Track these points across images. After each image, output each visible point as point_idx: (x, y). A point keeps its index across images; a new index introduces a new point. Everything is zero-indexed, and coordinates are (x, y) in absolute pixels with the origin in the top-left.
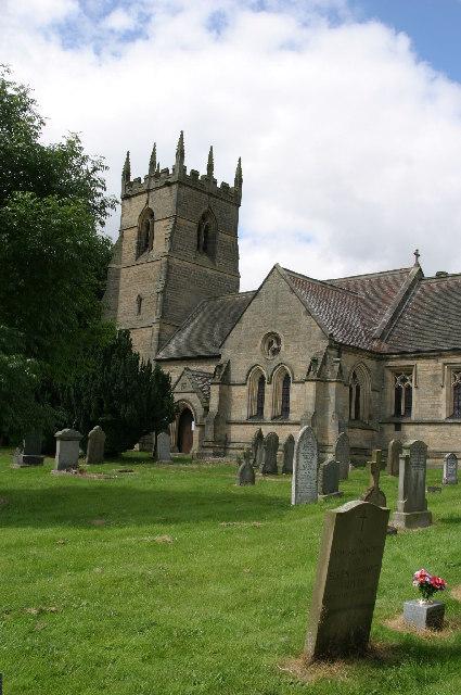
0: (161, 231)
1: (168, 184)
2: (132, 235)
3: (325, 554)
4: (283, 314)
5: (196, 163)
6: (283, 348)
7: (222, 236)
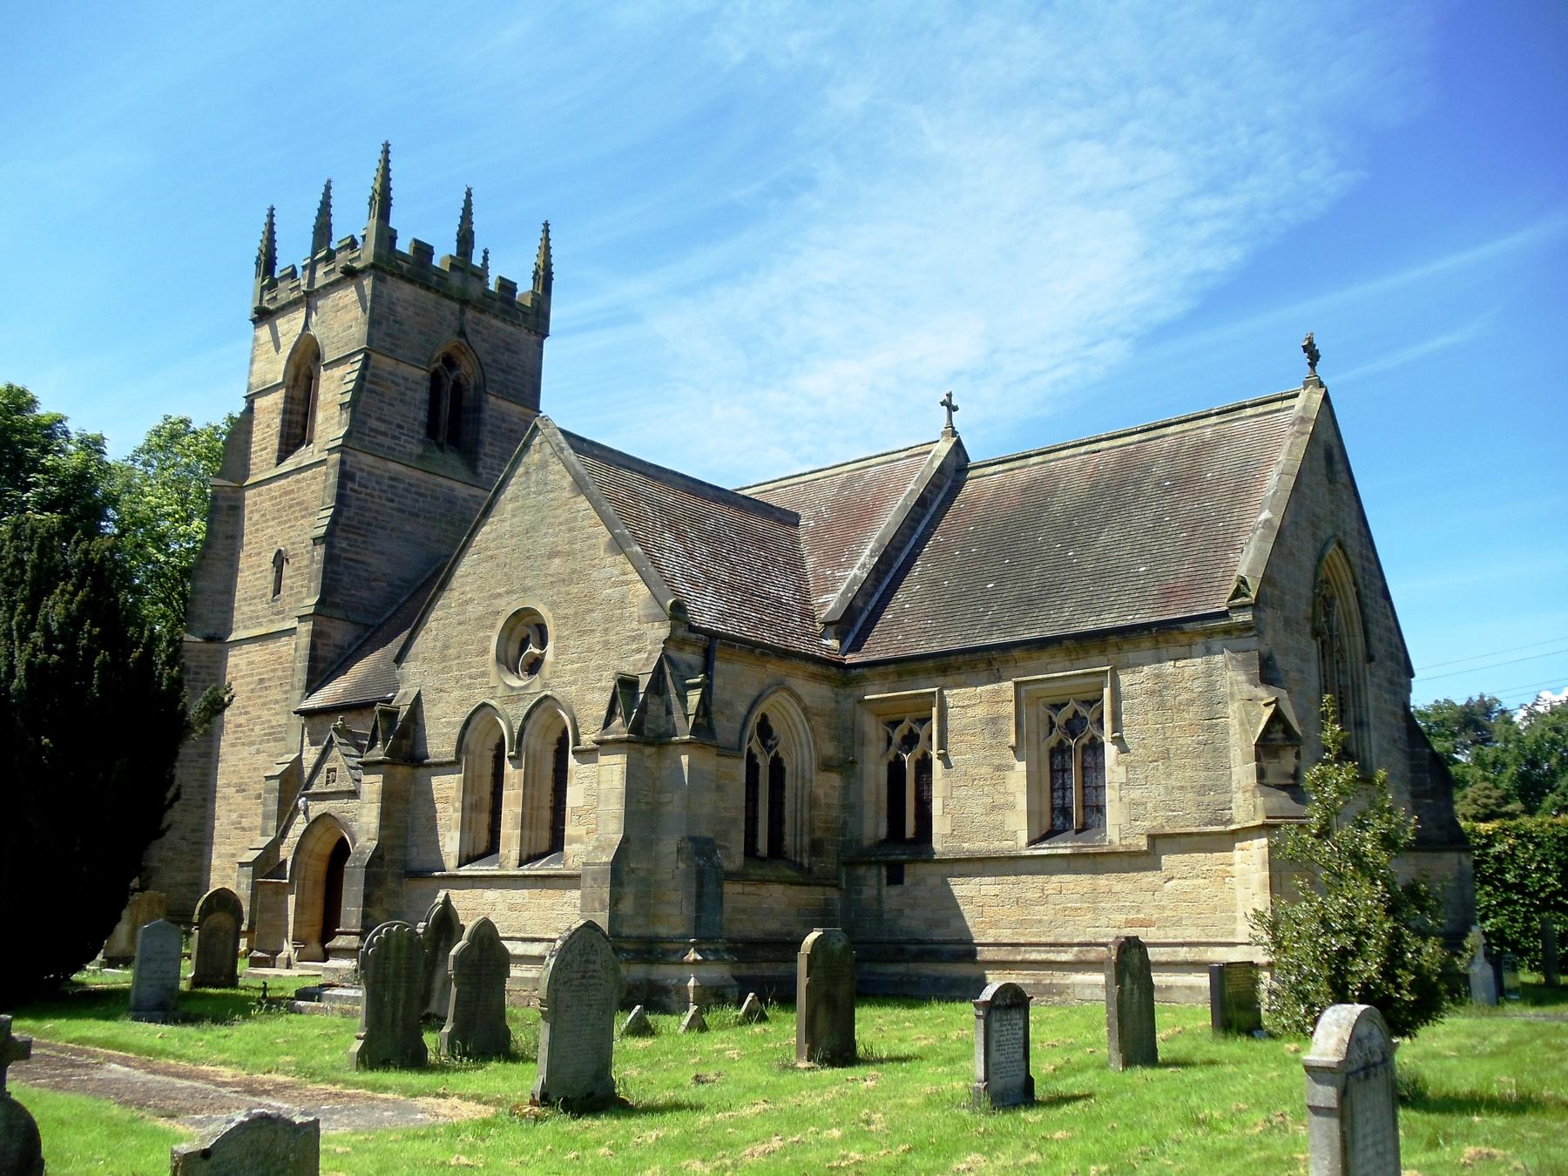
0: (334, 387)
1: (350, 274)
2: (270, 410)
3: (1258, 723)
4: (553, 555)
5: (424, 223)
6: (549, 657)
7: (495, 404)
